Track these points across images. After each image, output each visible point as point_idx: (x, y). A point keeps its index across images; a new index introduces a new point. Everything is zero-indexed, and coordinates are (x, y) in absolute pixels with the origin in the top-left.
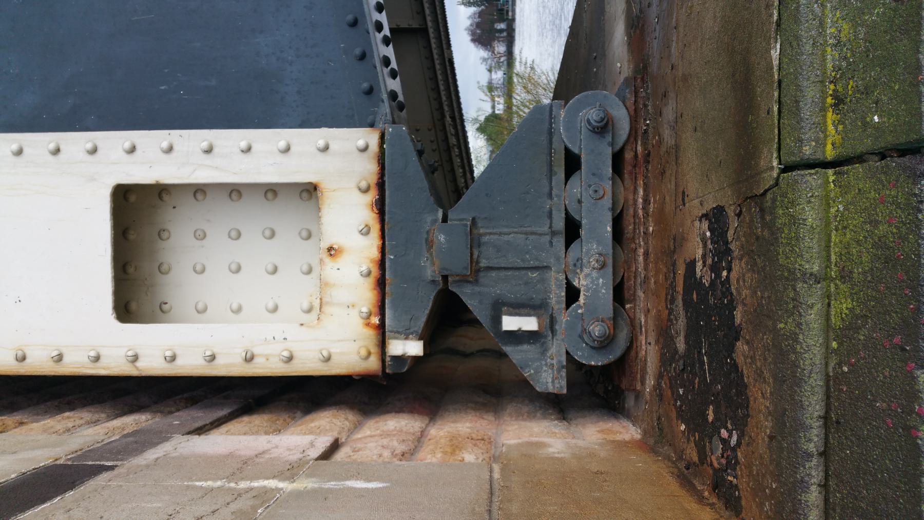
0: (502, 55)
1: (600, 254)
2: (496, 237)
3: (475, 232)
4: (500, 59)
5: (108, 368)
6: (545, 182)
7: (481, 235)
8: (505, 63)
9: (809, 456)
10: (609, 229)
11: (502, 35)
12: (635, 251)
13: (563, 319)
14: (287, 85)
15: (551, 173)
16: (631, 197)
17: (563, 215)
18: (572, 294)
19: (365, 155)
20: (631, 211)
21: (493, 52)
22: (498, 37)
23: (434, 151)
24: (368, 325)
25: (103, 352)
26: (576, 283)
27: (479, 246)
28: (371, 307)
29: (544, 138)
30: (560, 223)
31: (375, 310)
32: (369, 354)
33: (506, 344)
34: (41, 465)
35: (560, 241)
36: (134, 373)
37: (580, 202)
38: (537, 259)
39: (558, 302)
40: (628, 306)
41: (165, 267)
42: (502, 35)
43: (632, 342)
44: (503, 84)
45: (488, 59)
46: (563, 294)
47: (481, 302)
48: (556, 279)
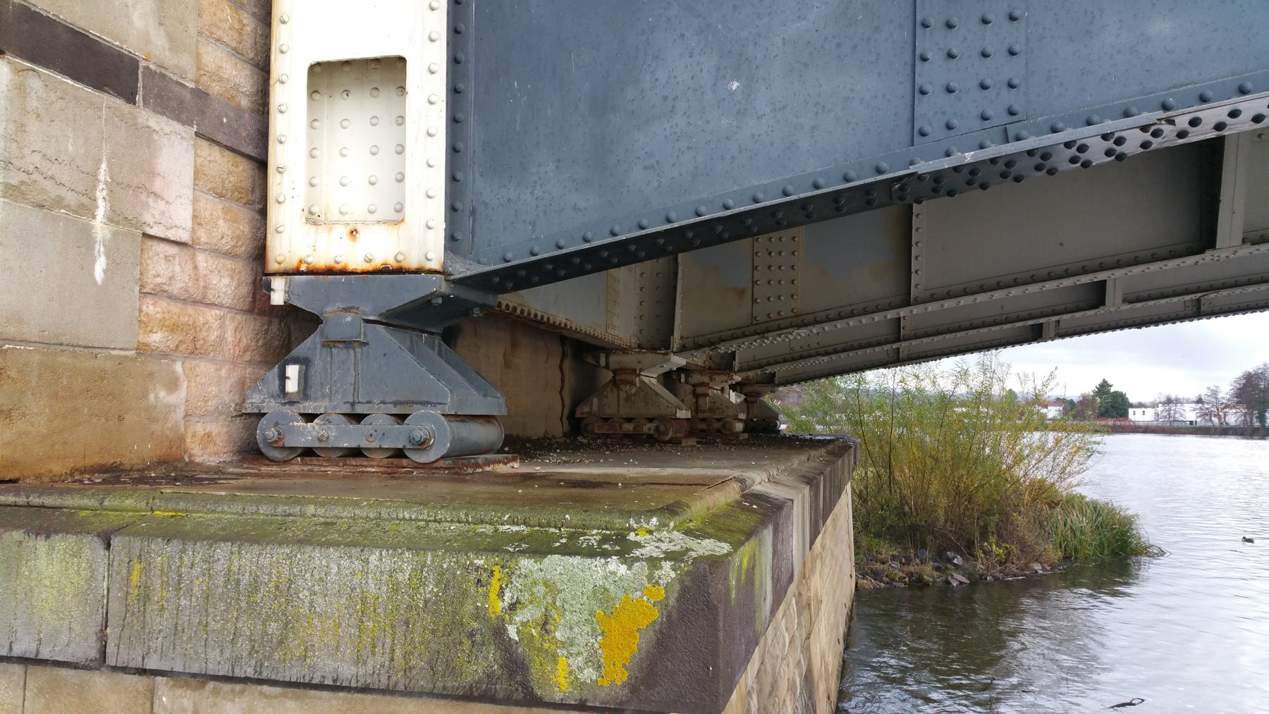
0: (1223, 420)
1: (328, 438)
2: (353, 361)
3: (356, 345)
4: (1215, 416)
5: (275, 61)
6: (393, 399)
7: (354, 349)
8: (1210, 424)
9: (28, 498)
10: (345, 445)
11: (1255, 420)
12: (337, 465)
13: (288, 410)
14: (515, 190)
15: (395, 404)
16: (375, 464)
17: (365, 412)
18: (310, 417)
19: (423, 258)
20: (365, 463)
21: (1227, 406)
22: (1251, 414)
23: (768, 315)
24: (301, 262)
25: (286, 56)
26: (316, 421)
27: (346, 348)
28: (313, 264)
29: (424, 398)
30: (360, 409)
31: (311, 267)
32: (280, 263)
33: (279, 368)
34: (137, 54)
35: (347, 409)
36: (272, 81)
37: (371, 424)
38: (336, 392)
39: (304, 407)
40: (299, 459)
41: (375, 93)
42: (1255, 420)
43: (273, 461)
44: (1174, 421)
45: (1216, 398)
46: (310, 412)
47: (309, 349)
48: (320, 407)
